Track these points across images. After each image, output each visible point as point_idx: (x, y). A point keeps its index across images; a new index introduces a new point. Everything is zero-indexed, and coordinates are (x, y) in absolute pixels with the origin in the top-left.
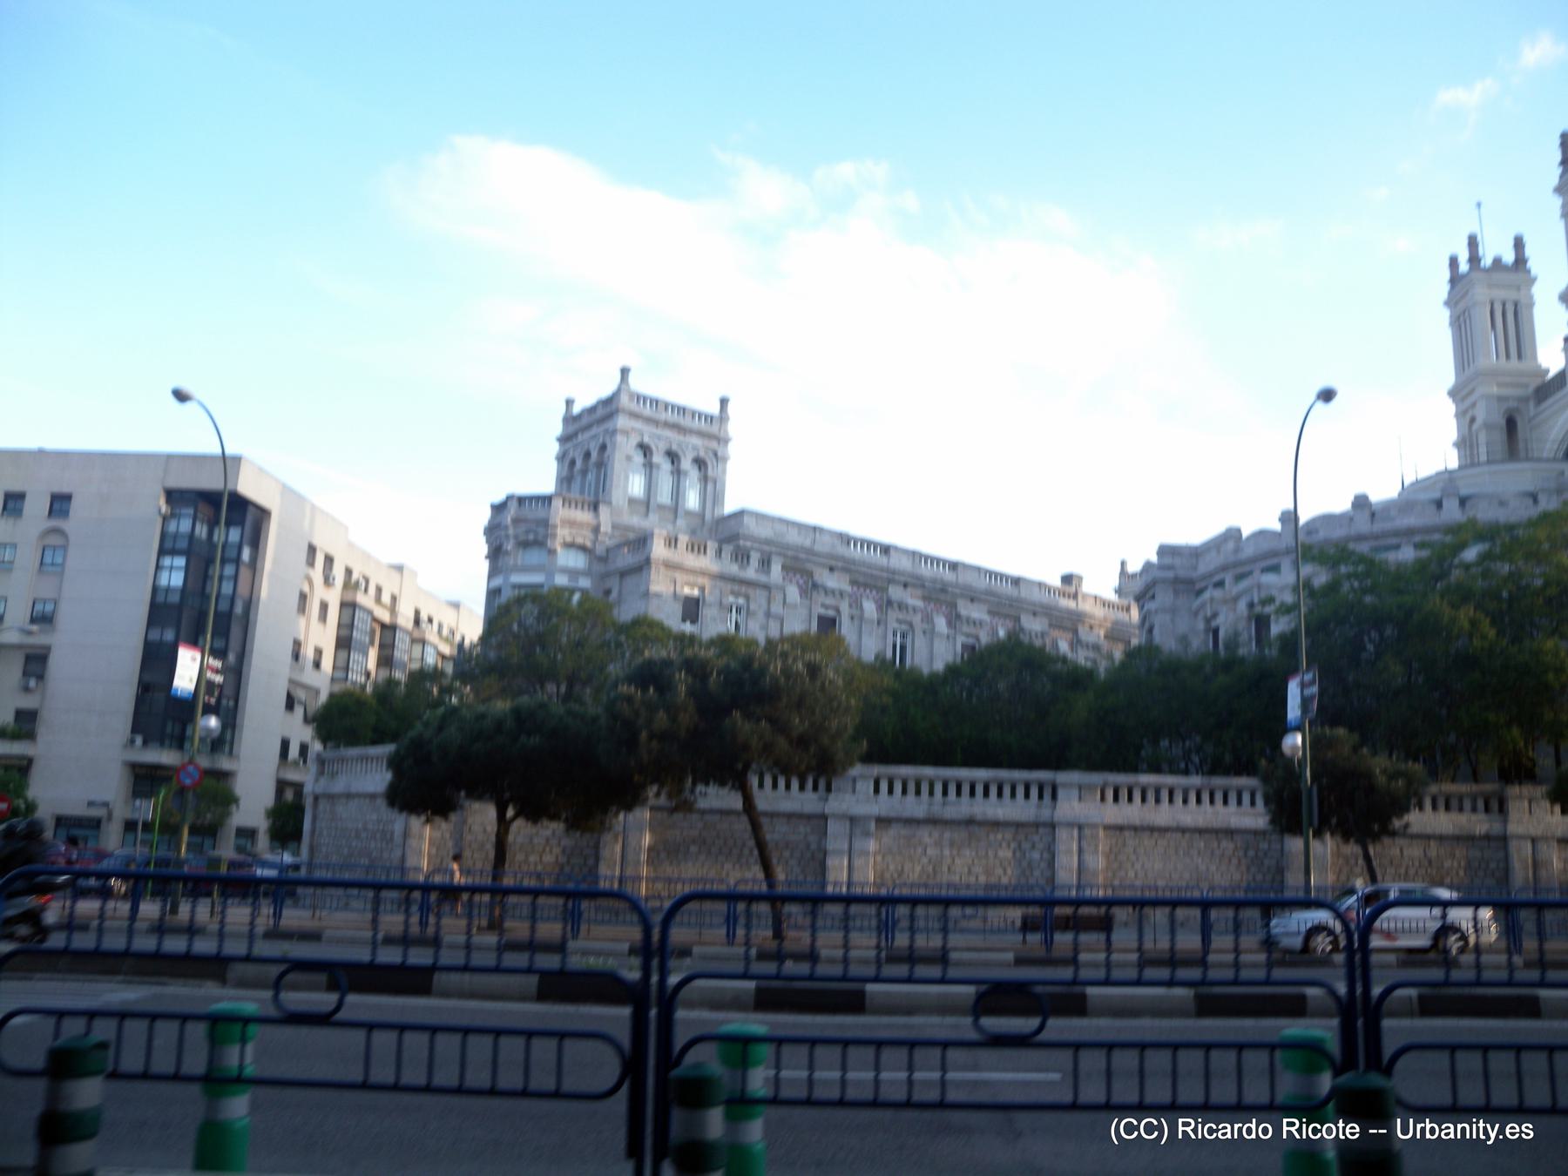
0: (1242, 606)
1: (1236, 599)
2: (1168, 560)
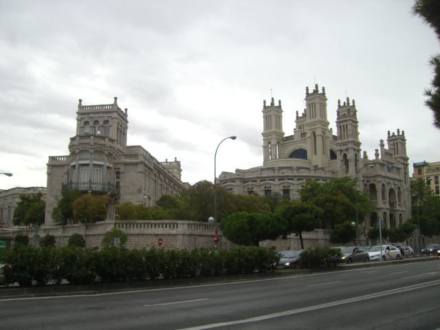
0: (262, 188)
1: (261, 186)
2: (239, 173)
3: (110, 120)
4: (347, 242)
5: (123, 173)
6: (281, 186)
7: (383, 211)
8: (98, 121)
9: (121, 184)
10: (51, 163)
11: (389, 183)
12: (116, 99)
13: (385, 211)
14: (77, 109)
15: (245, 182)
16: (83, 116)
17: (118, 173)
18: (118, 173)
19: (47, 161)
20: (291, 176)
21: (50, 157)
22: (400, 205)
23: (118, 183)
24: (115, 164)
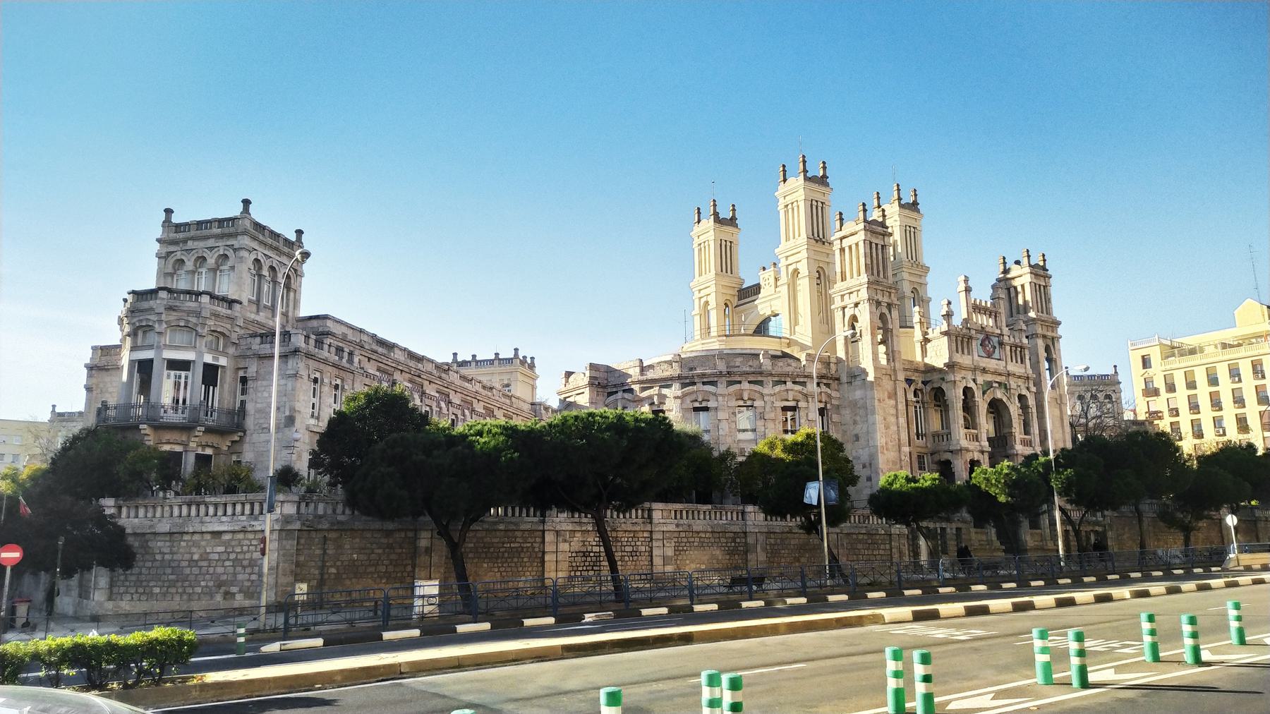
3: (230, 253)
4: (73, 443)
6: (688, 400)
7: (969, 457)
8: (204, 259)
9: (250, 407)
10: (96, 362)
11: (989, 385)
12: (246, 203)
13: (977, 456)
14: (158, 232)
15: (610, 394)
16: (172, 248)
17: (244, 380)
18: (244, 380)
19: (87, 356)
20: (710, 375)
21: (94, 348)
22: (1024, 443)
23: (243, 403)
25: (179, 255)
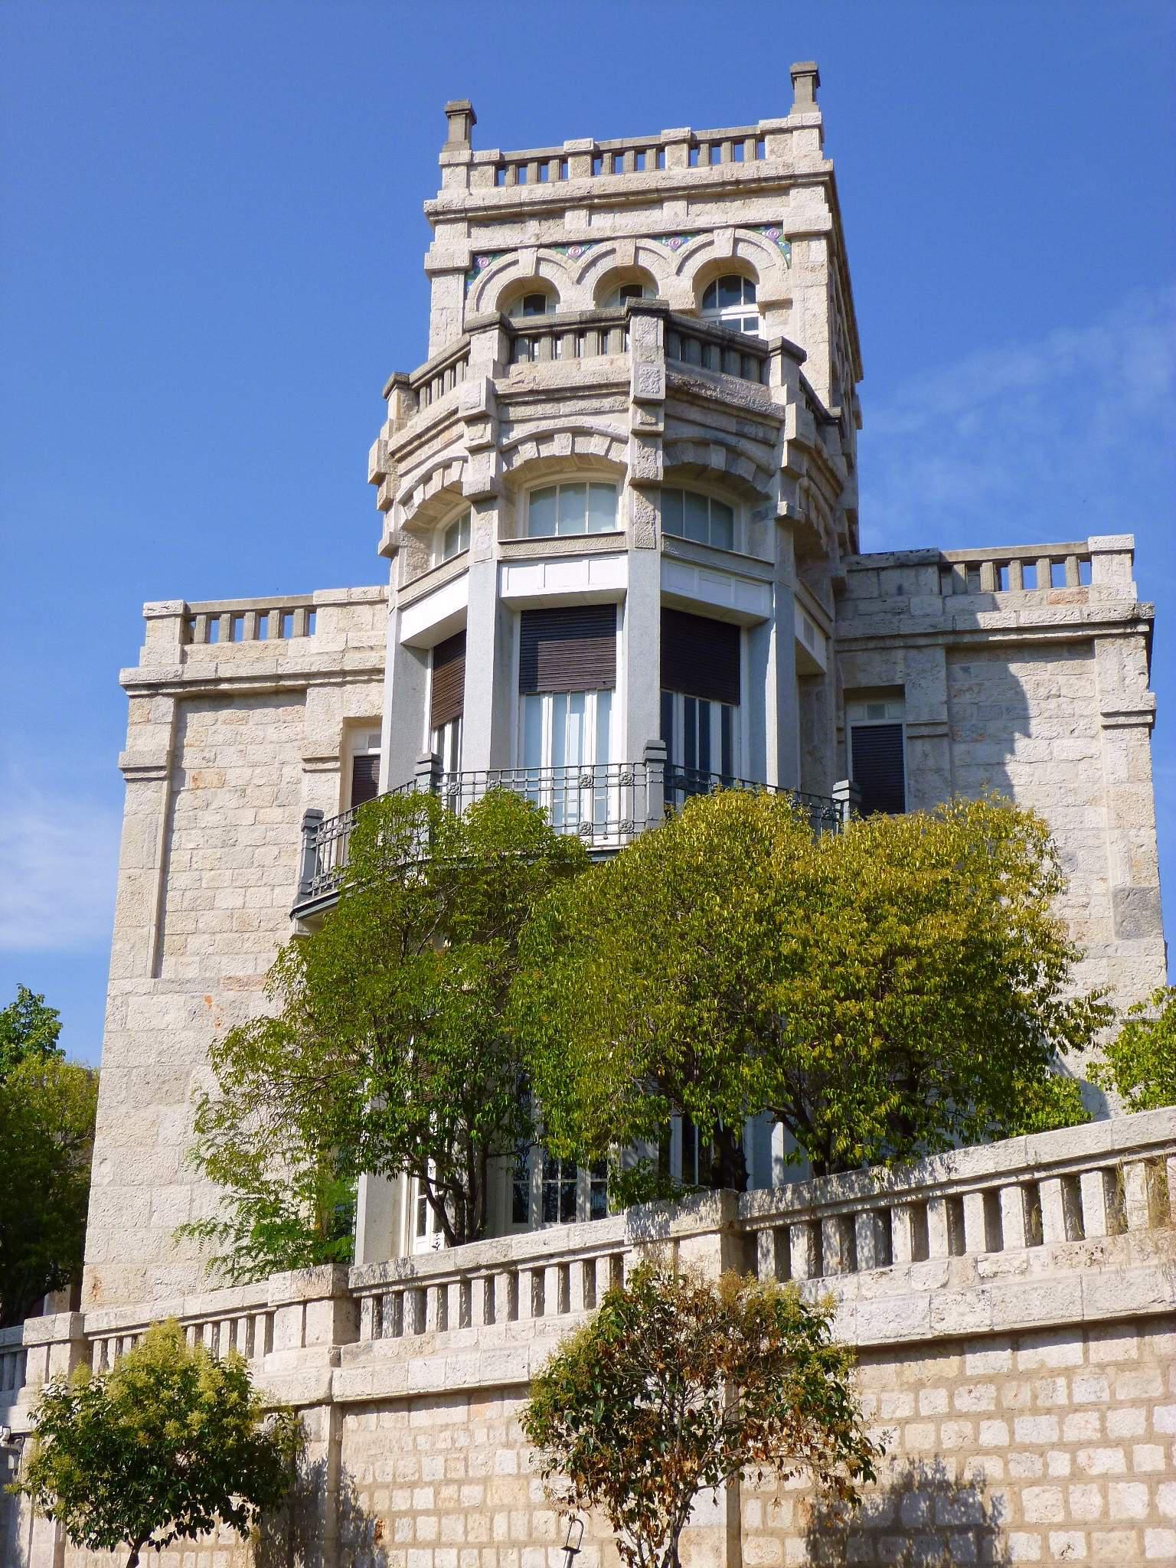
5: (944, 732)
24: (842, 646)
25: (524, 266)
